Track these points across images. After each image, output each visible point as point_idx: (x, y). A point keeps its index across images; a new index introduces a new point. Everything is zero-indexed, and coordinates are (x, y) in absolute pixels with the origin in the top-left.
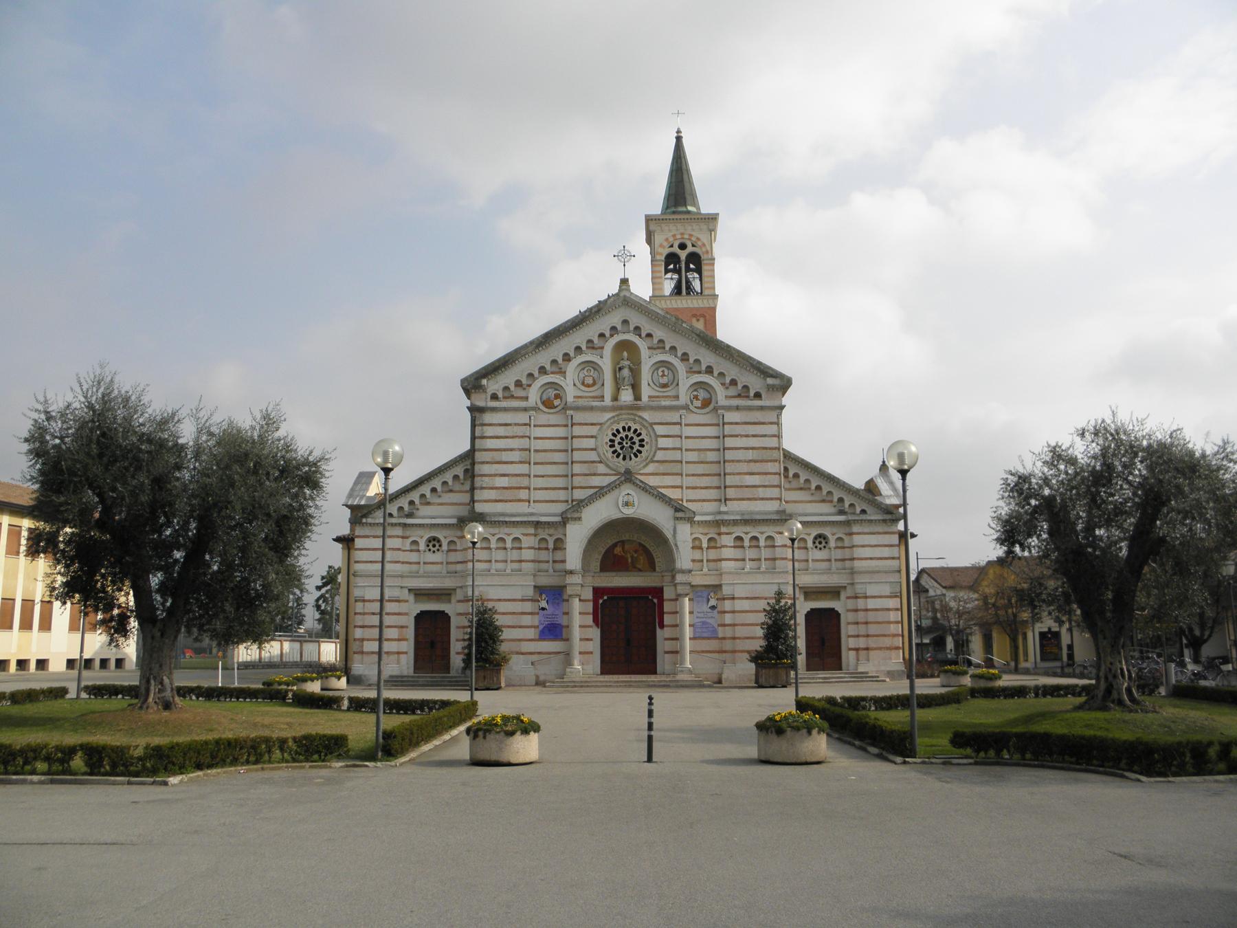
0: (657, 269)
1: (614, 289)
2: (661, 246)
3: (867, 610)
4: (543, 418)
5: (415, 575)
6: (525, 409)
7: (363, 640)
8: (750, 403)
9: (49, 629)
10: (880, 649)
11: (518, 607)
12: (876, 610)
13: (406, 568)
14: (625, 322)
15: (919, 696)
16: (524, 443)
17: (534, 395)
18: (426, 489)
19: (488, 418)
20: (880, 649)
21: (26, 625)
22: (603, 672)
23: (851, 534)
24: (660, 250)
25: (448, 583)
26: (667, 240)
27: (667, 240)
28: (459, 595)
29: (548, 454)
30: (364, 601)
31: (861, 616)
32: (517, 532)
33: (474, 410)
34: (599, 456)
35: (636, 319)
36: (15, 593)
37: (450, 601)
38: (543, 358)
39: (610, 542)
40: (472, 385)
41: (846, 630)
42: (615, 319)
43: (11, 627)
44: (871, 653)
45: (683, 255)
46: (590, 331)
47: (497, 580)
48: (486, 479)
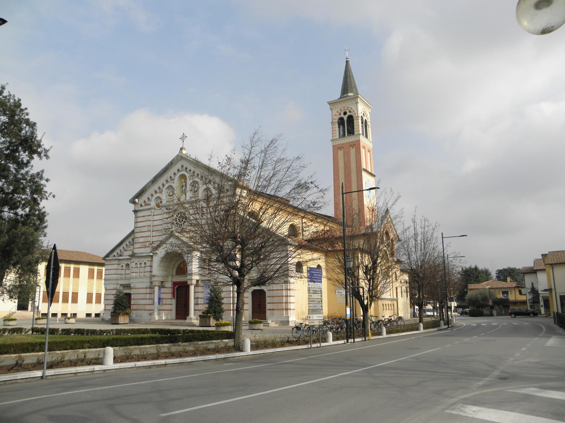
0: (334, 126)
1: (177, 152)
2: (335, 115)
3: (273, 290)
4: (157, 212)
5: (121, 279)
6: (149, 209)
9: (77, 302)
10: (278, 309)
11: (144, 291)
12: (278, 290)
13: (119, 276)
14: (182, 166)
15: (50, 329)
16: (150, 223)
17: (153, 204)
18: (124, 245)
19: (140, 214)
20: (278, 309)
21: (65, 300)
22: (177, 318)
24: (335, 117)
26: (337, 112)
27: (337, 112)
32: (145, 260)
33: (135, 212)
35: (186, 165)
36: (69, 290)
38: (156, 187)
39: (179, 262)
40: (133, 201)
41: (268, 300)
42: (178, 166)
43: (58, 302)
44: (275, 311)
46: (170, 173)
47: (139, 280)
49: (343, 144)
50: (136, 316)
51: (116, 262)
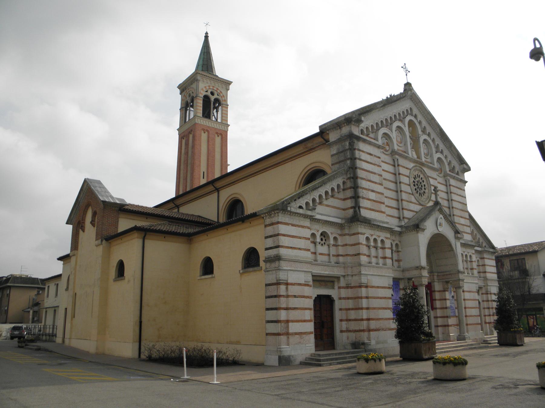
7: (287, 321)
8: (454, 175)
23: (484, 258)
25: (336, 272)
26: (205, 87)
27: (205, 87)
28: (343, 283)
29: (373, 185)
30: (287, 284)
31: (353, 326)
37: (333, 288)
45: (212, 98)
48: (365, 191)
49: (209, 127)
50: (378, 343)
51: (307, 223)
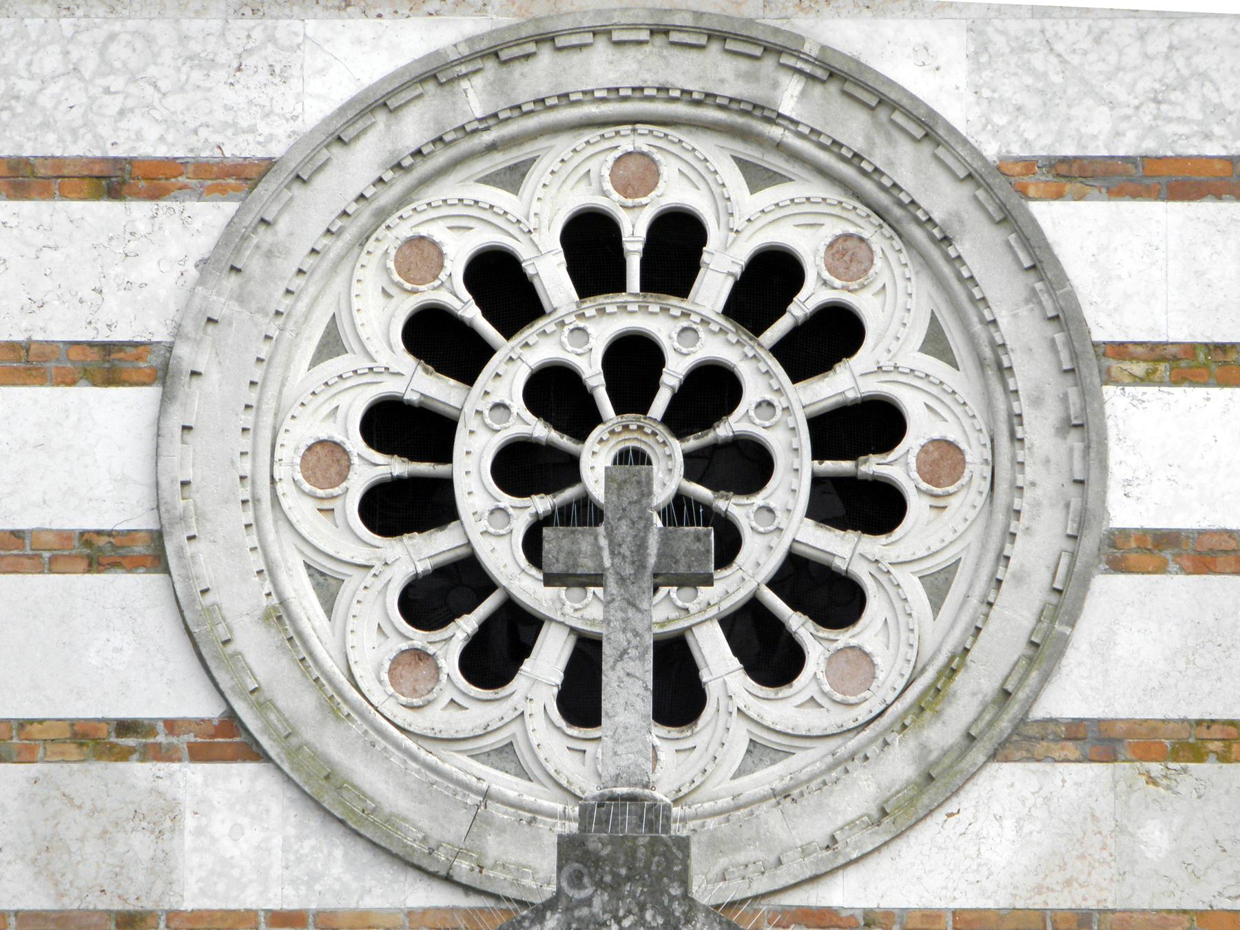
34: (203, 646)
